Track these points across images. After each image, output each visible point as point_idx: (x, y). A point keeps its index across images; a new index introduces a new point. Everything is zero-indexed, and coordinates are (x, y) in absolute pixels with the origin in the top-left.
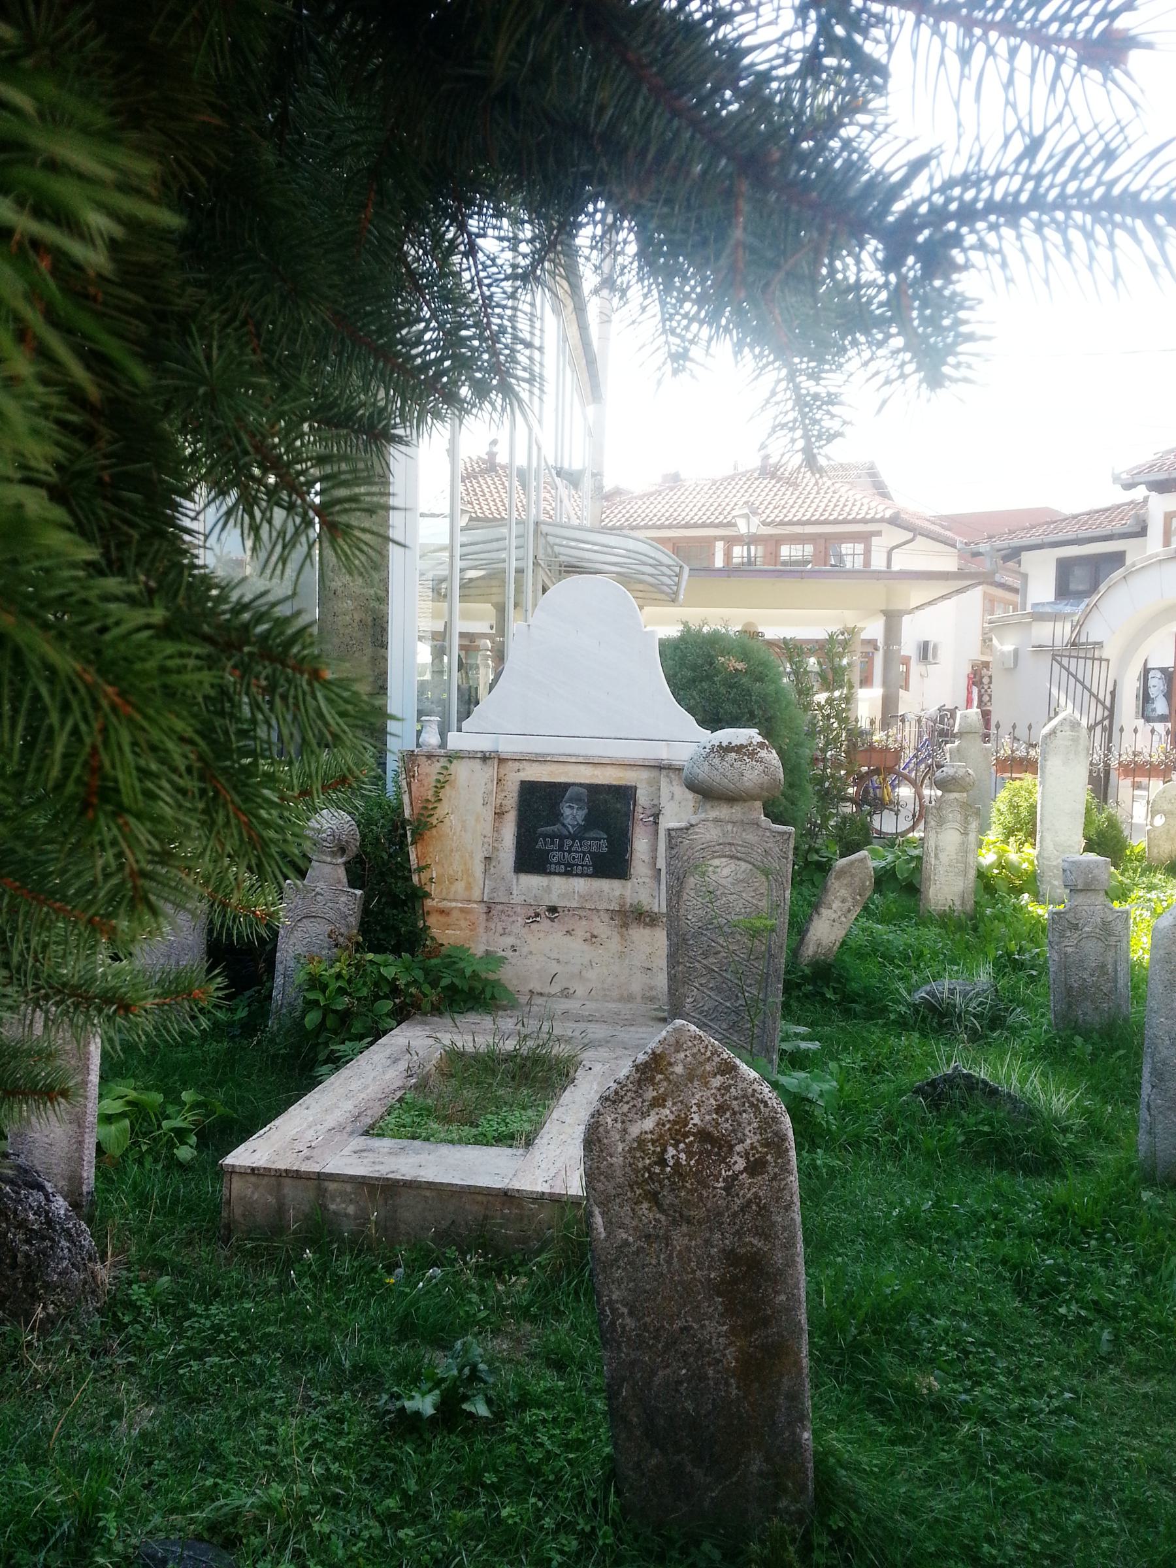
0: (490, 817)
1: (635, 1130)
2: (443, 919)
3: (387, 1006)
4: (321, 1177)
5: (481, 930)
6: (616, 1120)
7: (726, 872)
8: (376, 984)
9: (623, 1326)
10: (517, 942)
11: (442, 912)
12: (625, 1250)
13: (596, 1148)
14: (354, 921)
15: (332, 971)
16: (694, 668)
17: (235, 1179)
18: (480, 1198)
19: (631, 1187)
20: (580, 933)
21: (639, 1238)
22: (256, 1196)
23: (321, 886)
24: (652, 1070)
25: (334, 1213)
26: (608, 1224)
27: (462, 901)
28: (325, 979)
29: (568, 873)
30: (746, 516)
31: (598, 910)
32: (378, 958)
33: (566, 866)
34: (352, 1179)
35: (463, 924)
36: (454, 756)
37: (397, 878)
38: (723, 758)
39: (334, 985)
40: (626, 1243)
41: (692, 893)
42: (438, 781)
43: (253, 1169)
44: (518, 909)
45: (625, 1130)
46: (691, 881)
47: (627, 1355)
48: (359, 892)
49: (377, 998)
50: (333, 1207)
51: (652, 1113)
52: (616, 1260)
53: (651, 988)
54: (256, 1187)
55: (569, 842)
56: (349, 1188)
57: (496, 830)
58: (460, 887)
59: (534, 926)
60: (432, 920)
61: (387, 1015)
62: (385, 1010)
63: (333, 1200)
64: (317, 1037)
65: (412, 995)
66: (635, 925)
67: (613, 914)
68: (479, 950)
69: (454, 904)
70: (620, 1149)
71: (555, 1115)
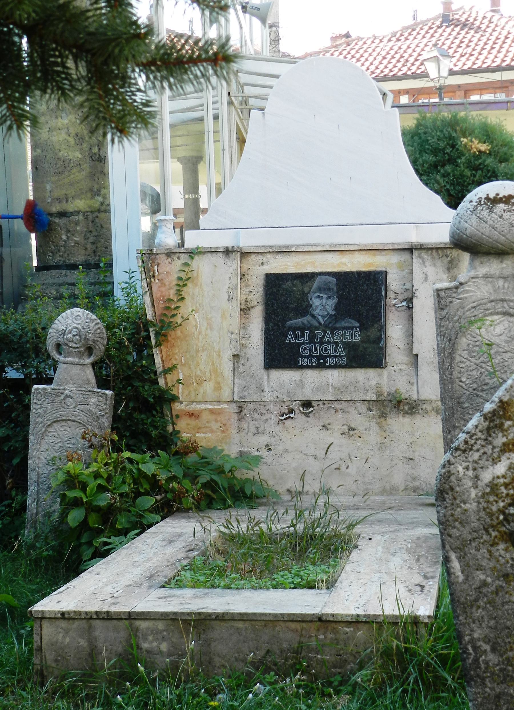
0: (236, 313)
1: (487, 476)
2: (193, 422)
3: (148, 501)
4: (131, 616)
5: (233, 431)
6: (467, 468)
7: (499, 329)
8: (135, 481)
9: (487, 663)
10: (272, 441)
11: (191, 415)
12: (484, 590)
13: (449, 497)
14: (106, 422)
15: (91, 470)
16: (435, 151)
17: (45, 624)
18: (293, 625)
19: (487, 530)
20: (337, 427)
21: (498, 578)
22: (67, 640)
23: (69, 388)
24: (500, 417)
25: (148, 652)
26: (465, 568)
27: (211, 402)
28: (83, 478)
29: (321, 366)
30: (436, 59)
31: (354, 402)
32: (135, 456)
33: (318, 358)
34: (164, 616)
35: (215, 426)
36: (192, 253)
37: (144, 381)
38: (491, 210)
39: (93, 484)
40: (484, 584)
41: (465, 354)
42: (180, 279)
43: (63, 614)
44: (271, 406)
45: (477, 477)
46: (464, 342)
47: (492, 689)
48: (109, 393)
49: (138, 494)
50: (145, 645)
51: (503, 458)
52: (476, 600)
53: (414, 479)
54: (67, 632)
55: (319, 334)
56: (161, 625)
57: (243, 326)
58: (208, 387)
59: (288, 422)
60: (182, 425)
61: (150, 511)
62: (148, 506)
63: (145, 639)
64: (79, 538)
65: (173, 491)
66: (393, 415)
67: (369, 404)
68: (233, 451)
69: (203, 406)
70: (473, 495)
71: (348, 568)
